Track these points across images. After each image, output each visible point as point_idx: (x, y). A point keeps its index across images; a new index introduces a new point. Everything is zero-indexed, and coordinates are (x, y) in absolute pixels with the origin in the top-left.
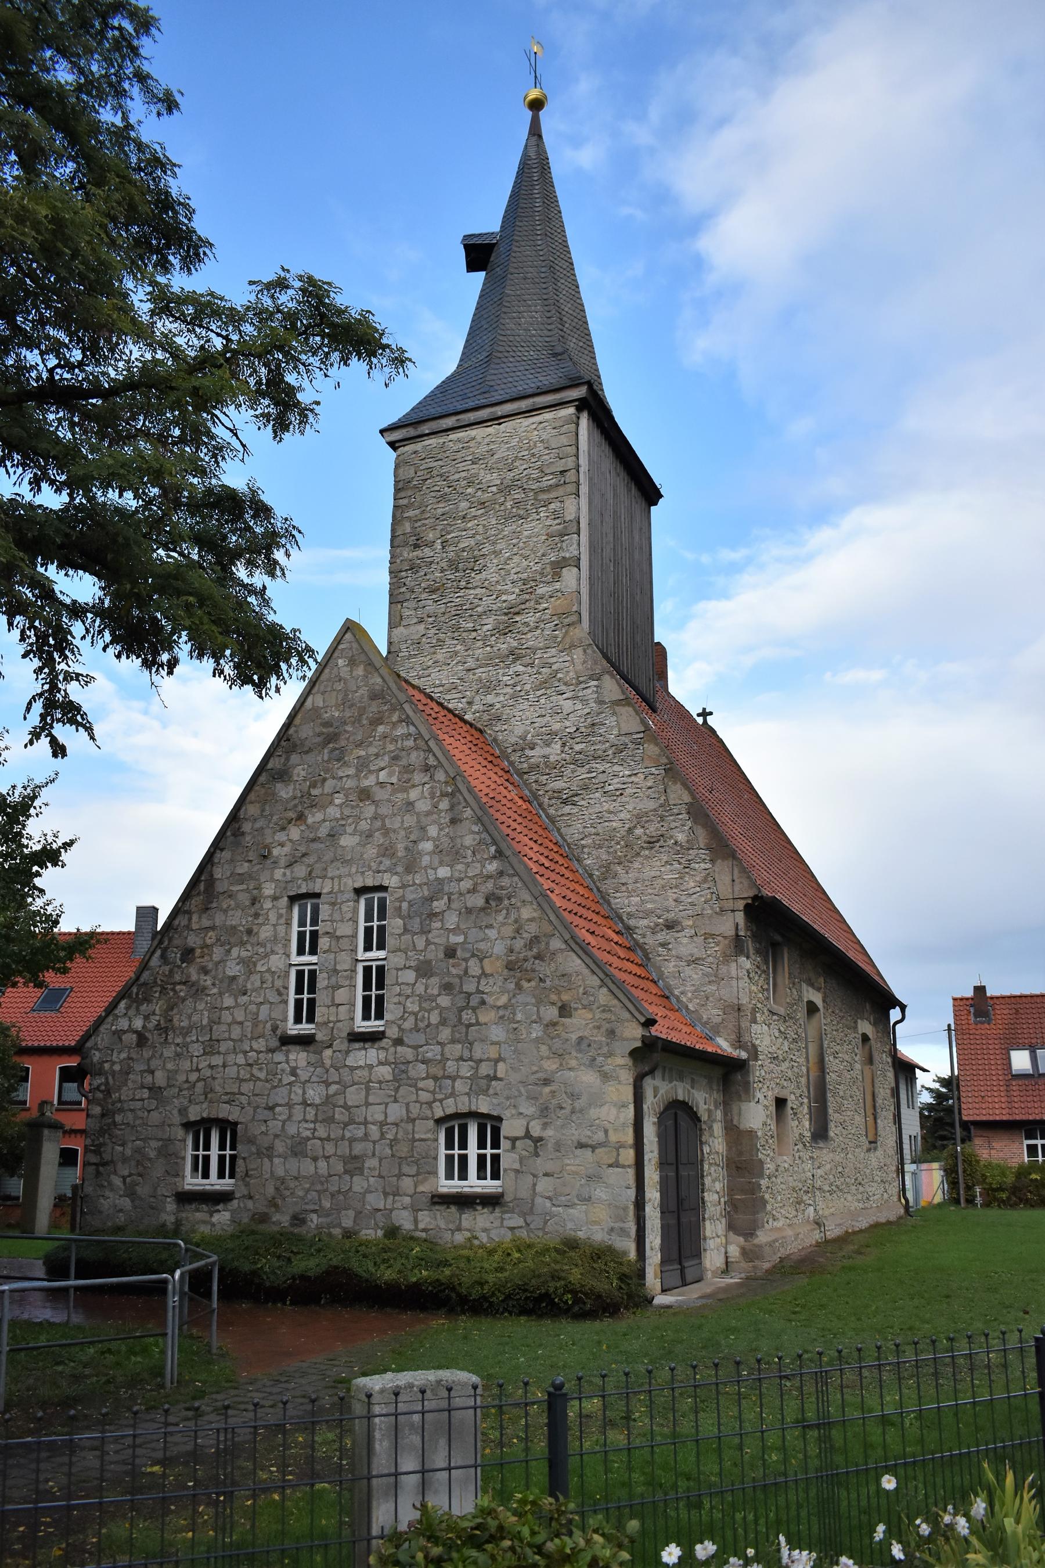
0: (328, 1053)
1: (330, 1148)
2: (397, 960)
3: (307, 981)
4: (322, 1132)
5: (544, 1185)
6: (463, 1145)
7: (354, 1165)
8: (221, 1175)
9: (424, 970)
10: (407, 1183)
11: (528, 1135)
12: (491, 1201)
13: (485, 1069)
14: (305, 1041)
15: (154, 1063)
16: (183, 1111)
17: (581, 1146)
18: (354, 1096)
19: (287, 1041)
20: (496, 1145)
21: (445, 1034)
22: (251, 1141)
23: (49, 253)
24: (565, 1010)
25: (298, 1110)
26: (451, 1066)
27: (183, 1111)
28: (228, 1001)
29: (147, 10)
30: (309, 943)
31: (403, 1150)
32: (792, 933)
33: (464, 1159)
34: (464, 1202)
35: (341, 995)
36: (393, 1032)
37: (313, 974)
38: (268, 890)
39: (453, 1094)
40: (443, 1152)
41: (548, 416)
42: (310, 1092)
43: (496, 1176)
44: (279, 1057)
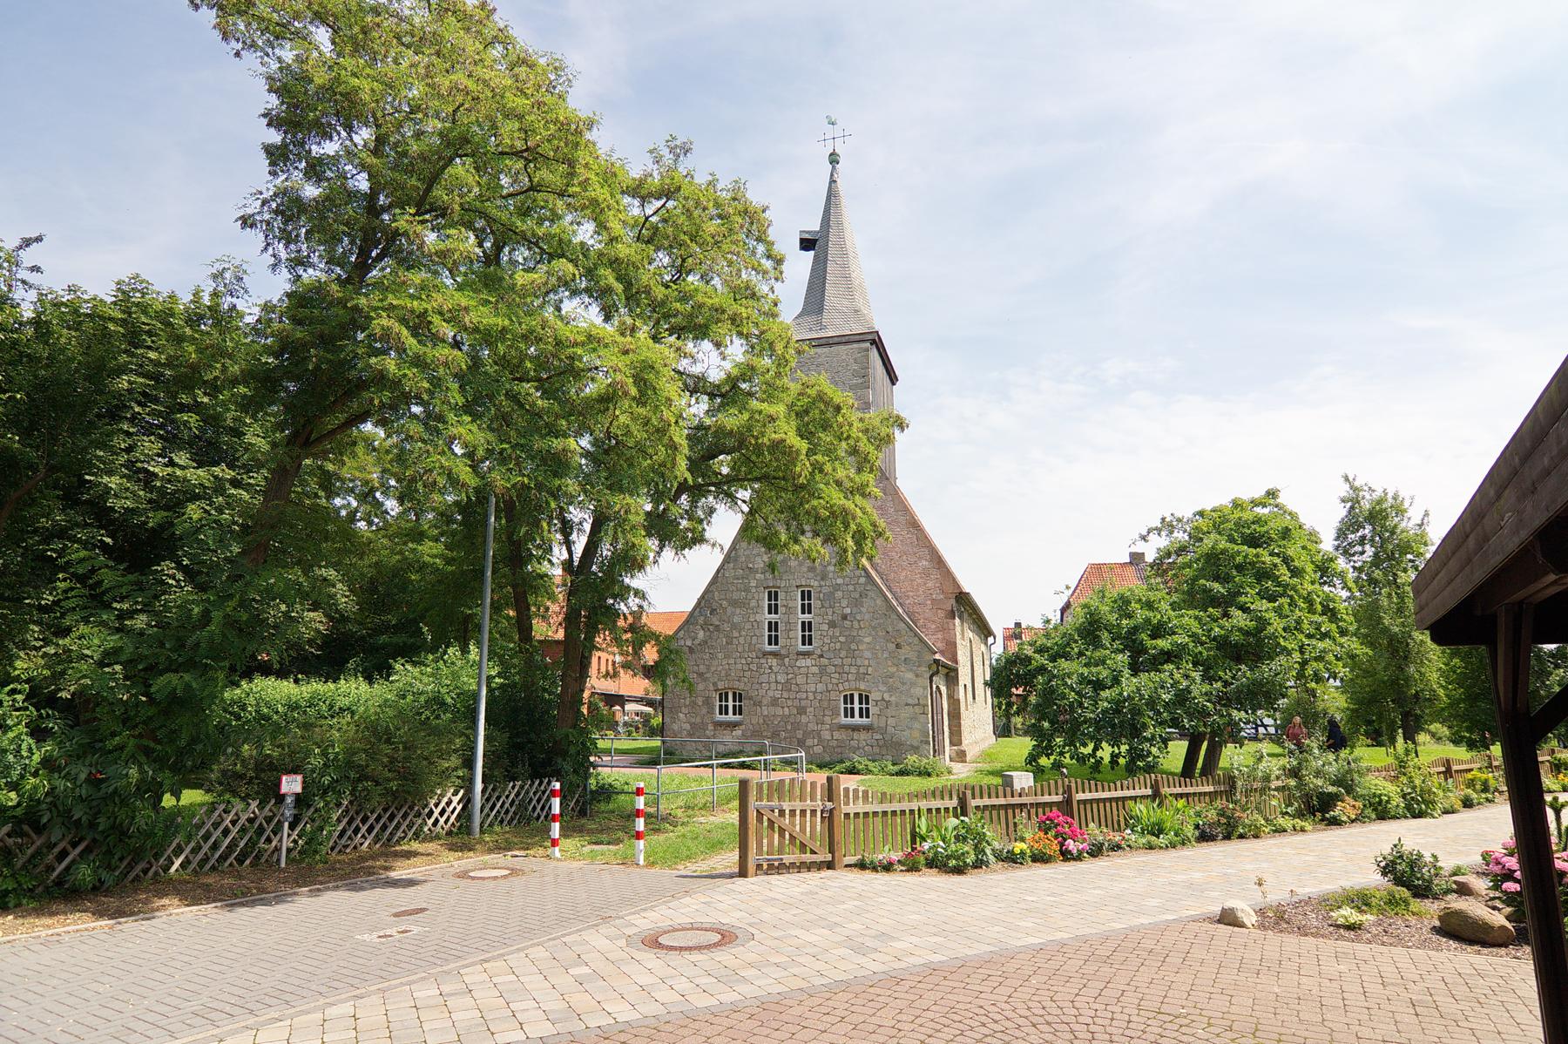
3: (773, 626)
7: (802, 711)
9: (832, 625)
10: (827, 719)
12: (867, 728)
13: (862, 670)
16: (715, 684)
18: (800, 680)
19: (765, 654)
21: (843, 653)
22: (751, 698)
25: (773, 686)
26: (846, 669)
27: (715, 684)
28: (736, 634)
34: (855, 728)
35: (792, 634)
36: (818, 652)
38: (753, 583)
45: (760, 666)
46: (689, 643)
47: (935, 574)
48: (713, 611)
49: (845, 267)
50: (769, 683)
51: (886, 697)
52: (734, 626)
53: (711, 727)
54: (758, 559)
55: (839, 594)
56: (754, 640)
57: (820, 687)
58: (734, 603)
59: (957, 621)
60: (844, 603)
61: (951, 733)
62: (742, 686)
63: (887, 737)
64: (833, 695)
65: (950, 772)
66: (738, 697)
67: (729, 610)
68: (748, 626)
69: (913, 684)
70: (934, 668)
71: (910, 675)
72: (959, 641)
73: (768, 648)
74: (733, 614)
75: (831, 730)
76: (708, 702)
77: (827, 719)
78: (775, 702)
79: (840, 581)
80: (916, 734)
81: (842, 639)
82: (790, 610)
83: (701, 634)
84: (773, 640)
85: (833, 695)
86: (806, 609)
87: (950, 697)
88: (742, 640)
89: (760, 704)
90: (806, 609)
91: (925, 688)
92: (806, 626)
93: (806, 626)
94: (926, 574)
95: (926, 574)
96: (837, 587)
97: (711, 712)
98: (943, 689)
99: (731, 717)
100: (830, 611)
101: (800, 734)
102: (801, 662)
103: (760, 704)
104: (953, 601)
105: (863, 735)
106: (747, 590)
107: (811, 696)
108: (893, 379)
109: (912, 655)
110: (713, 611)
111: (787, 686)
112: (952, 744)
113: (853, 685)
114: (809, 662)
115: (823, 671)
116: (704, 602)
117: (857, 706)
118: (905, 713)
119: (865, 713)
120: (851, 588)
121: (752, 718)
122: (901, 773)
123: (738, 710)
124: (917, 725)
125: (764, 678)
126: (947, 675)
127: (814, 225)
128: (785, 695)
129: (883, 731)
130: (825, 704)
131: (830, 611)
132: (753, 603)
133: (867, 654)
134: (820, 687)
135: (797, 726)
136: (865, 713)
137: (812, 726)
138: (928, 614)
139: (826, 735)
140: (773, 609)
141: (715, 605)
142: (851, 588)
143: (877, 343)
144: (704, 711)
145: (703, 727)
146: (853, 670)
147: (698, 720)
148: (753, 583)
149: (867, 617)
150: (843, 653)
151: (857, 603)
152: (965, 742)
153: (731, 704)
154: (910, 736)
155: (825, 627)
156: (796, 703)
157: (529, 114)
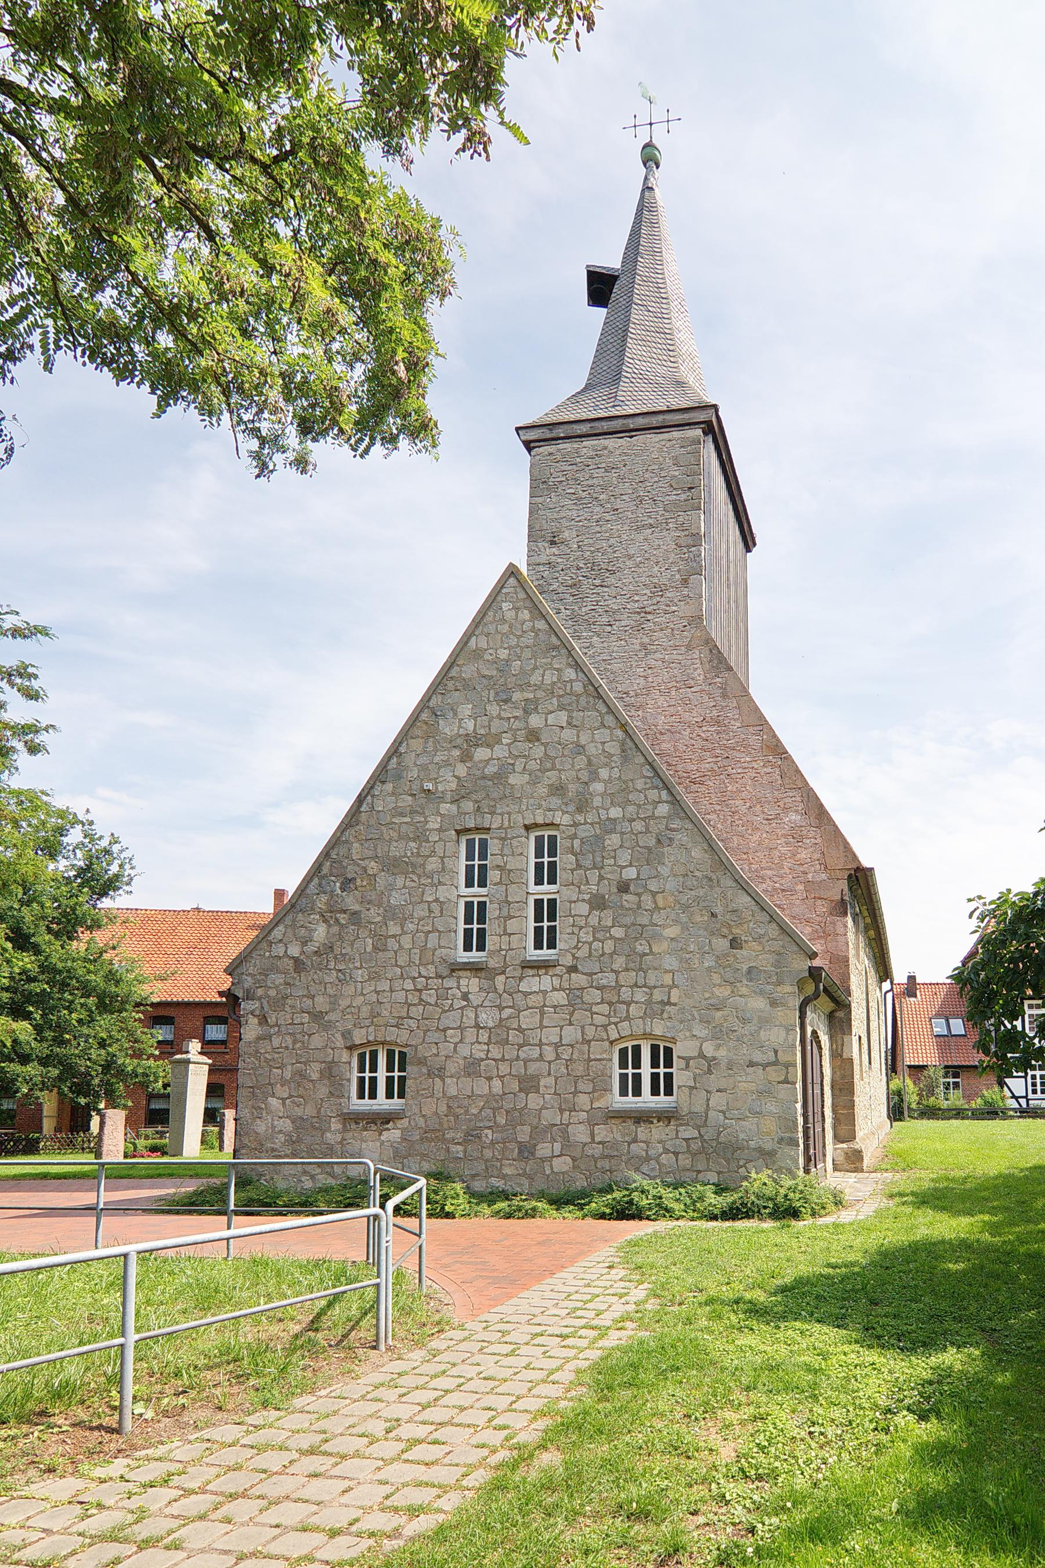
1: (504, 1068)
2: (571, 893)
3: (476, 912)
4: (495, 1052)
5: (717, 1101)
6: (374, 1068)
7: (529, 1084)
8: (389, 1095)
9: (598, 903)
10: (583, 1100)
11: (702, 1055)
12: (666, 1116)
13: (658, 995)
14: (475, 969)
16: (346, 1035)
17: (751, 1064)
18: (528, 1020)
19: (456, 968)
20: (669, 1064)
21: (619, 962)
22: (422, 1062)
25: (470, 1035)
26: (626, 993)
27: (346, 1035)
28: (394, 929)
31: (579, 1069)
33: (373, 1081)
34: (642, 1117)
35: (512, 925)
36: (568, 961)
37: (482, 905)
38: (434, 823)
39: (628, 1018)
40: (617, 1071)
41: (676, 434)
43: (669, 1092)
45: (443, 994)
46: (294, 951)
47: (813, 837)
48: (347, 884)
49: (663, 316)
50: (462, 1029)
51: (709, 1049)
52: (391, 913)
53: (336, 1125)
54: (446, 774)
55: (613, 840)
56: (433, 940)
57: (571, 1034)
58: (393, 865)
59: (849, 920)
60: (624, 858)
61: (836, 1120)
62: (403, 1037)
63: (709, 1134)
64: (597, 1050)
65: (838, 1203)
66: (399, 1059)
67: (381, 881)
68: (420, 911)
69: (765, 1022)
70: (810, 989)
71: (759, 1003)
72: (852, 961)
73: (463, 956)
74: (391, 887)
75: (592, 1123)
76: (331, 1073)
77: (583, 1100)
78: (472, 1068)
79: (615, 813)
80: (770, 1125)
81: (618, 932)
82: (510, 877)
83: (320, 932)
84: (476, 940)
85: (597, 1050)
86: (546, 874)
87: (837, 1055)
88: (406, 941)
89: (440, 1073)
90: (546, 874)
91: (789, 1029)
92: (546, 910)
93: (546, 910)
94: (796, 837)
95: (796, 837)
96: (610, 826)
97: (338, 1091)
98: (824, 1039)
99: (382, 1102)
100: (593, 876)
101: (523, 1134)
102: (532, 983)
103: (440, 1073)
104: (844, 885)
105: (658, 1132)
106: (420, 837)
107: (549, 1053)
108: (748, 541)
109: (765, 962)
110: (347, 884)
111: (499, 1035)
112: (837, 1138)
113: (638, 1027)
114: (546, 982)
115: (575, 999)
116: (331, 866)
117: (646, 1071)
118: (748, 1082)
119: (663, 1085)
120: (638, 826)
121: (423, 1106)
122: (732, 1214)
123: (397, 1088)
124: (771, 1107)
125: (451, 1020)
126: (831, 1016)
127: (612, 260)
128: (495, 1052)
129: (701, 1121)
130: (579, 1069)
131: (593, 876)
132: (433, 864)
133: (670, 962)
134: (571, 1034)
135: (517, 1116)
136: (663, 1085)
137: (550, 1116)
138: (799, 909)
139: (580, 1134)
140: (477, 877)
141: (351, 871)
142: (638, 826)
143: (714, 430)
144: (323, 1091)
145: (319, 1125)
146: (640, 996)
147: (309, 1111)
148: (434, 823)
149: (671, 885)
150: (619, 962)
151: (650, 857)
152: (860, 1134)
153: (382, 1075)
154: (757, 1130)
155: (583, 908)
156: (519, 1068)
157: (770, 1113)
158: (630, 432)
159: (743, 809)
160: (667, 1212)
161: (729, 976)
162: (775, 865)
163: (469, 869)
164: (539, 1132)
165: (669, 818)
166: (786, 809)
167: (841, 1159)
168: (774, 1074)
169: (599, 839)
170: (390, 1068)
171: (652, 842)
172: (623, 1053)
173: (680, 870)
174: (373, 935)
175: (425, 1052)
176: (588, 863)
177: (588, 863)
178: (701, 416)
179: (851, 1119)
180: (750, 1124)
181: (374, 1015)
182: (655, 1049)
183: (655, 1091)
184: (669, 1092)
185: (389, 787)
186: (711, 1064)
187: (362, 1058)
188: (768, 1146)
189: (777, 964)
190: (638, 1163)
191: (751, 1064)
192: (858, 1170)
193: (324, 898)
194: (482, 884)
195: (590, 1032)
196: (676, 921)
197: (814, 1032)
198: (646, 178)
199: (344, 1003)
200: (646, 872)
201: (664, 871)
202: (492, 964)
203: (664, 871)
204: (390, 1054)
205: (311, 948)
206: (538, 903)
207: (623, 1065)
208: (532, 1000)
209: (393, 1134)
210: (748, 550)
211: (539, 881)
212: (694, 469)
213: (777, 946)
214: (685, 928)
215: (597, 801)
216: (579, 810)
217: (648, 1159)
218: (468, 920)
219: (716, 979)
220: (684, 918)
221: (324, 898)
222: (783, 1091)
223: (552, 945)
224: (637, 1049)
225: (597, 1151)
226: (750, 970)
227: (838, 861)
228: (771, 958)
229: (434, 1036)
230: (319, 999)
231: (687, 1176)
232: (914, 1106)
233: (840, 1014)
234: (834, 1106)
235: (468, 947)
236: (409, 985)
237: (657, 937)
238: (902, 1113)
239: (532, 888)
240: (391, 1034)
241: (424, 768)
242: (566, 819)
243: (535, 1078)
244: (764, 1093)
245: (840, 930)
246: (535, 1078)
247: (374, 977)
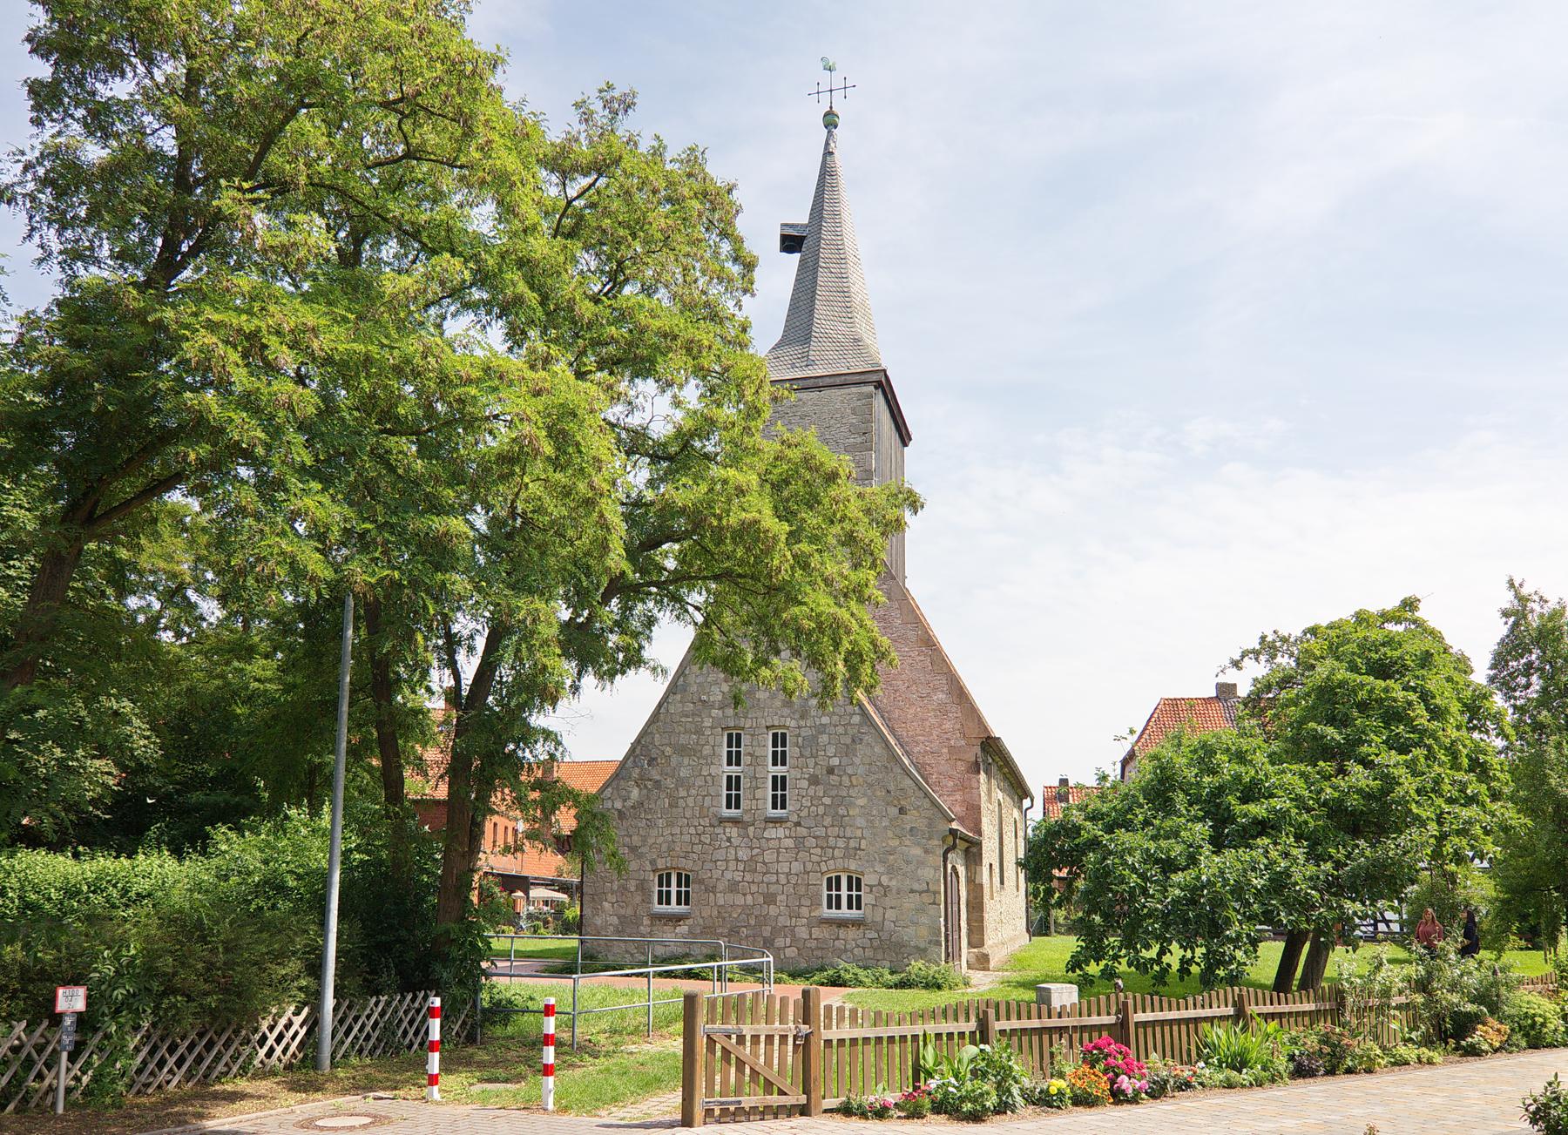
0: (751, 829)
1: (754, 888)
2: (795, 773)
3: (733, 783)
4: (748, 877)
5: (890, 914)
6: (669, 885)
7: (770, 899)
8: (679, 903)
9: (814, 780)
10: (804, 911)
11: (880, 884)
12: (857, 923)
13: (853, 844)
14: (735, 821)
15: (631, 831)
16: (653, 862)
17: (912, 891)
18: (769, 857)
19: (722, 821)
20: (859, 889)
21: (828, 821)
22: (701, 882)
23: (291, 87)
24: (902, 811)
25: (732, 865)
26: (832, 842)
27: (653, 862)
28: (683, 793)
29: (693, 161)
30: (734, 759)
31: (802, 890)
32: (992, 755)
33: (668, 893)
34: (842, 923)
35: (759, 793)
36: (795, 818)
37: (738, 778)
38: (708, 723)
39: (833, 858)
40: (825, 893)
41: (854, 389)
42: (740, 853)
43: (859, 908)
44: (718, 830)
46: (618, 805)
47: (955, 712)
49: (842, 277)
52: (681, 782)
53: (646, 921)
55: (824, 739)
58: (682, 750)
59: (983, 776)
60: (831, 750)
61: (970, 931)
65: (967, 984)
66: (684, 880)
67: (674, 760)
68: (700, 782)
69: (921, 864)
71: (917, 851)
73: (726, 813)
74: (680, 765)
75: (810, 926)
76: (643, 887)
77: (804, 911)
78: (733, 887)
80: (924, 932)
81: (827, 801)
82: (756, 760)
91: (936, 869)
92: (779, 783)
93: (779, 783)
94: (942, 711)
95: (942, 711)
96: (821, 729)
98: (961, 870)
99: (673, 907)
100: (811, 762)
102: (771, 833)
103: (713, 890)
104: (978, 749)
105: (852, 933)
108: (904, 437)
109: (921, 824)
111: (751, 865)
112: (970, 945)
113: (840, 863)
114: (781, 832)
120: (840, 730)
121: (702, 910)
122: (902, 985)
123: (684, 898)
124: (924, 920)
125: (720, 854)
128: (748, 877)
131: (811, 762)
133: (861, 822)
135: (762, 920)
137: (782, 921)
139: (803, 933)
140: (734, 759)
142: (840, 730)
143: (884, 386)
146: (841, 843)
147: (629, 911)
148: (708, 723)
150: (828, 821)
151: (848, 751)
154: (914, 934)
155: (805, 784)
158: (819, 388)
159: (903, 688)
160: (860, 983)
161: (898, 831)
162: (925, 734)
163: (729, 753)
164: (776, 931)
165: (860, 725)
166: (935, 689)
167: (973, 960)
168: (927, 898)
169: (814, 738)
170: (679, 885)
171: (849, 741)
172: (829, 880)
173: (867, 760)
174: (669, 796)
175: (702, 875)
176: (807, 753)
177: (807, 753)
178: (875, 378)
179: (981, 930)
180: (911, 930)
181: (670, 850)
182: (850, 879)
183: (850, 907)
184: (859, 908)
185: (678, 697)
186: (887, 890)
187: (660, 877)
188: (922, 946)
189: (930, 825)
190: (840, 953)
191: (912, 891)
192: (984, 969)
193: (637, 770)
194: (738, 764)
195: (809, 866)
196: (865, 795)
197: (954, 868)
198: (827, 144)
199: (651, 841)
200: (845, 761)
201: (857, 761)
202: (746, 818)
203: (857, 761)
204: (679, 875)
205: (629, 803)
206: (774, 778)
207: (829, 888)
208: (772, 844)
209: (683, 929)
210: (905, 445)
211: (775, 764)
212: (867, 418)
213: (929, 813)
214: (870, 800)
215: (813, 713)
216: (802, 717)
217: (846, 951)
218: (729, 788)
219: (890, 834)
220: (869, 792)
221: (637, 770)
222: (932, 910)
223: (783, 807)
224: (838, 879)
225: (814, 944)
226: (912, 829)
227: (975, 732)
228: (925, 821)
229: (708, 866)
230: (635, 838)
231: (870, 962)
232: (1061, 920)
233: (974, 850)
234: (968, 919)
235: (729, 807)
236: (692, 830)
237: (852, 804)
238: (1048, 928)
239: (771, 768)
240: (682, 863)
241: (700, 685)
242: (793, 724)
243: (774, 895)
244: (921, 910)
245: (975, 785)
246: (774, 895)
247: (670, 824)
